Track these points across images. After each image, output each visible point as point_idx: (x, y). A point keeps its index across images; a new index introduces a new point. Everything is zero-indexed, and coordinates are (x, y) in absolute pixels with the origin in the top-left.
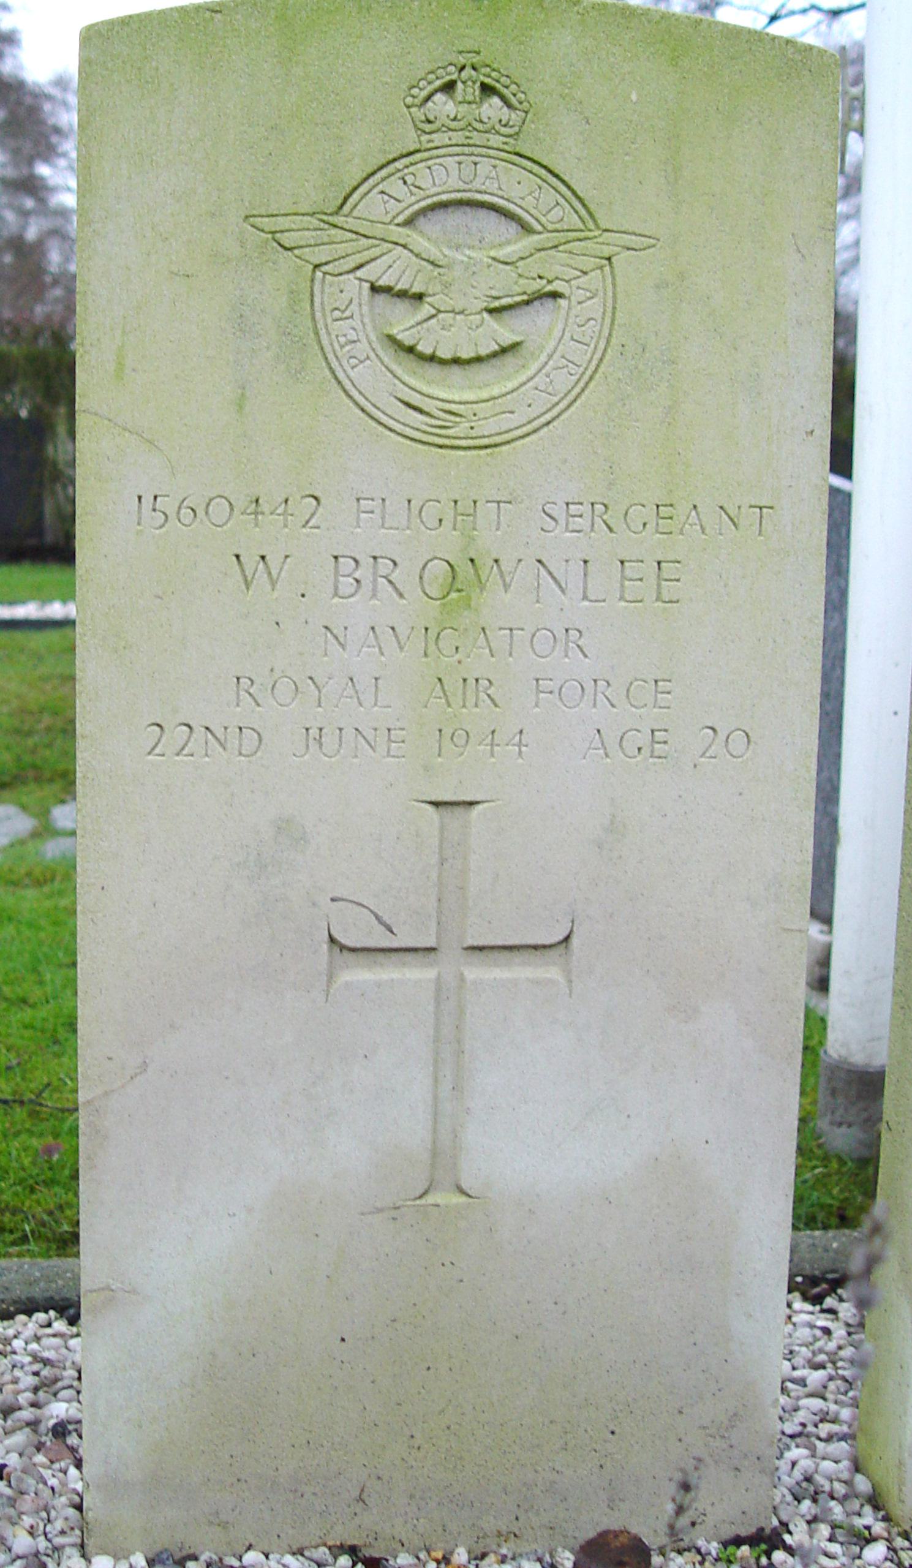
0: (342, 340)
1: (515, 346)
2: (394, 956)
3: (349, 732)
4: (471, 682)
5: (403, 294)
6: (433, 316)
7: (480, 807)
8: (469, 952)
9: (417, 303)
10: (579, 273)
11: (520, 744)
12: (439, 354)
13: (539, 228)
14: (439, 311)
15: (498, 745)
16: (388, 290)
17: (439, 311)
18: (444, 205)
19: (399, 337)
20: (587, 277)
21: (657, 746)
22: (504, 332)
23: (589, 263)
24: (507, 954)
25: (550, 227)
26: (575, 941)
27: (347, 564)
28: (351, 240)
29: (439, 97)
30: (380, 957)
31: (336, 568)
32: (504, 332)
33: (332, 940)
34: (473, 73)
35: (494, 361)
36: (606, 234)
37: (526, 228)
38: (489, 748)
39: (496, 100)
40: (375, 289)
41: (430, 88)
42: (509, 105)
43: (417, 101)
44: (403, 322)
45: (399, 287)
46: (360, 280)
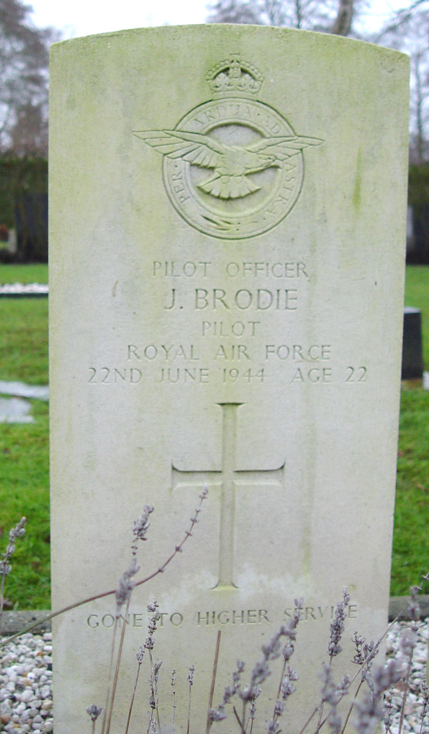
0: (177, 189)
1: (257, 191)
2: (264, 474)
3: (182, 372)
4: (236, 347)
5: (205, 167)
6: (219, 177)
7: (240, 407)
8: (237, 473)
9: (210, 172)
10: (287, 157)
11: (262, 376)
12: (213, 192)
13: (268, 136)
14: (222, 175)
15: (252, 376)
16: (198, 165)
17: (222, 175)
18: (227, 125)
19: (203, 187)
20: (291, 159)
21: (203, 377)
22: (252, 185)
23: (291, 152)
24: (213, 474)
25: (274, 135)
26: (286, 467)
27: (201, 293)
28: (181, 142)
29: (222, 75)
30: (257, 474)
31: (215, 294)
32: (252, 185)
33: (174, 469)
34: (237, 63)
35: (248, 197)
36: (300, 138)
37: (263, 136)
38: (247, 378)
39: (247, 76)
40: (192, 165)
41: (218, 71)
42: (254, 78)
43: (212, 77)
44: (205, 180)
45: (202, 165)
46: (185, 160)
